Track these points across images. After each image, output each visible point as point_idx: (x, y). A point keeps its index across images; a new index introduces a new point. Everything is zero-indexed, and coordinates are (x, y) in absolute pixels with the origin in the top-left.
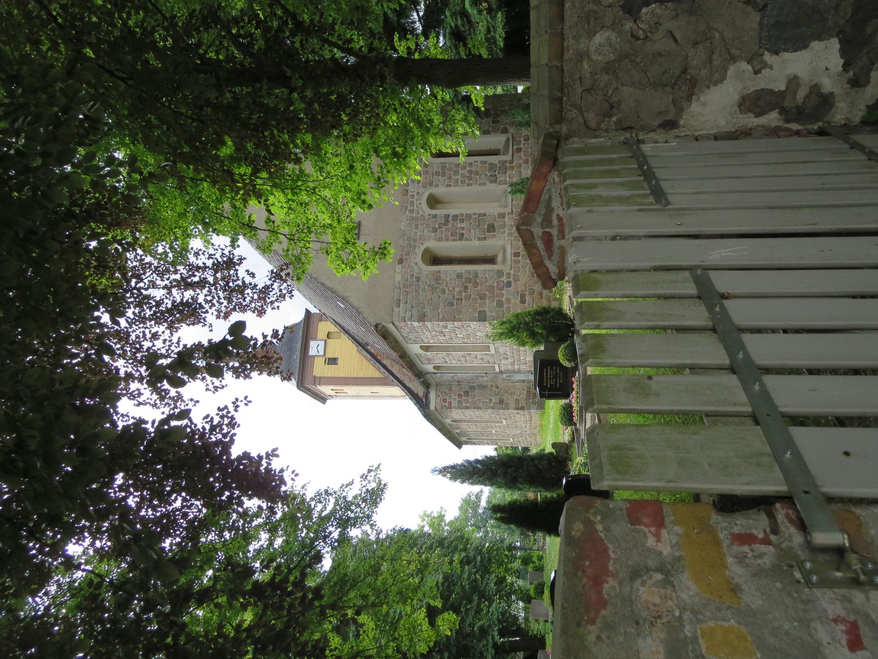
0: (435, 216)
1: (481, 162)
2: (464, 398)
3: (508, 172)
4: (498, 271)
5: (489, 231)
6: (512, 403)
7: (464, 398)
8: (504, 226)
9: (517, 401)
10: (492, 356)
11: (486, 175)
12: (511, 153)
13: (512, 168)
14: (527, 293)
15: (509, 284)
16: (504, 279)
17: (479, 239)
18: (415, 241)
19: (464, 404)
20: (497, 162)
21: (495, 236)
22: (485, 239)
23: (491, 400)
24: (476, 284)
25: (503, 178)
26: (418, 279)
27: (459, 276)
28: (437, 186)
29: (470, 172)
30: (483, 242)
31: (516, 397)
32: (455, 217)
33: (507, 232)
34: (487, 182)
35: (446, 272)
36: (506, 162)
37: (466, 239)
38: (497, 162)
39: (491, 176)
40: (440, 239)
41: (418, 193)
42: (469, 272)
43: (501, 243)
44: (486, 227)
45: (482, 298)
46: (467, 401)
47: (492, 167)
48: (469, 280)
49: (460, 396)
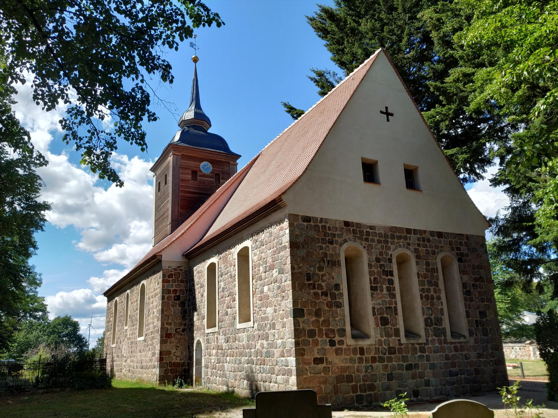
0: (390, 261)
1: (442, 309)
2: (173, 295)
3: (436, 338)
4: (344, 330)
5: (382, 318)
6: (168, 347)
7: (173, 295)
8: (388, 335)
9: (169, 353)
10: (233, 324)
11: (432, 315)
12: (453, 341)
13: (440, 343)
14: (325, 365)
15: (332, 343)
16: (337, 339)
17: (374, 308)
18: (367, 240)
19: (166, 296)
20: (443, 326)
21: (377, 325)
22: (374, 314)
23: (170, 324)
24: (329, 305)
25: (431, 333)
26: (331, 243)
27: (337, 287)
28: (417, 263)
29: (432, 297)
30: (370, 311)
31: (173, 351)
32: (391, 282)
33: (383, 339)
34: (425, 316)
35: (339, 273)
36: (445, 336)
37: (372, 295)
38: (443, 326)
39: (431, 320)
40: (370, 266)
41: (409, 244)
42: (342, 295)
43: (372, 333)
44: (385, 315)
45: (318, 314)
46: (168, 298)
47: (439, 321)
48: (333, 296)
49: (175, 291)
